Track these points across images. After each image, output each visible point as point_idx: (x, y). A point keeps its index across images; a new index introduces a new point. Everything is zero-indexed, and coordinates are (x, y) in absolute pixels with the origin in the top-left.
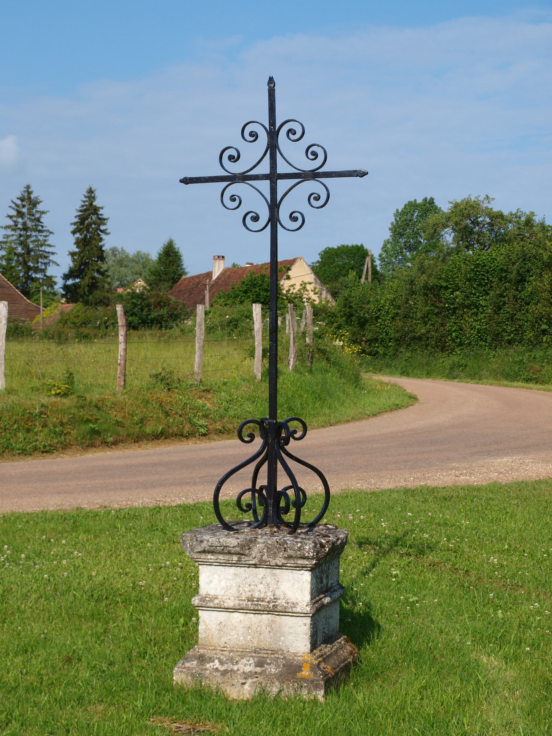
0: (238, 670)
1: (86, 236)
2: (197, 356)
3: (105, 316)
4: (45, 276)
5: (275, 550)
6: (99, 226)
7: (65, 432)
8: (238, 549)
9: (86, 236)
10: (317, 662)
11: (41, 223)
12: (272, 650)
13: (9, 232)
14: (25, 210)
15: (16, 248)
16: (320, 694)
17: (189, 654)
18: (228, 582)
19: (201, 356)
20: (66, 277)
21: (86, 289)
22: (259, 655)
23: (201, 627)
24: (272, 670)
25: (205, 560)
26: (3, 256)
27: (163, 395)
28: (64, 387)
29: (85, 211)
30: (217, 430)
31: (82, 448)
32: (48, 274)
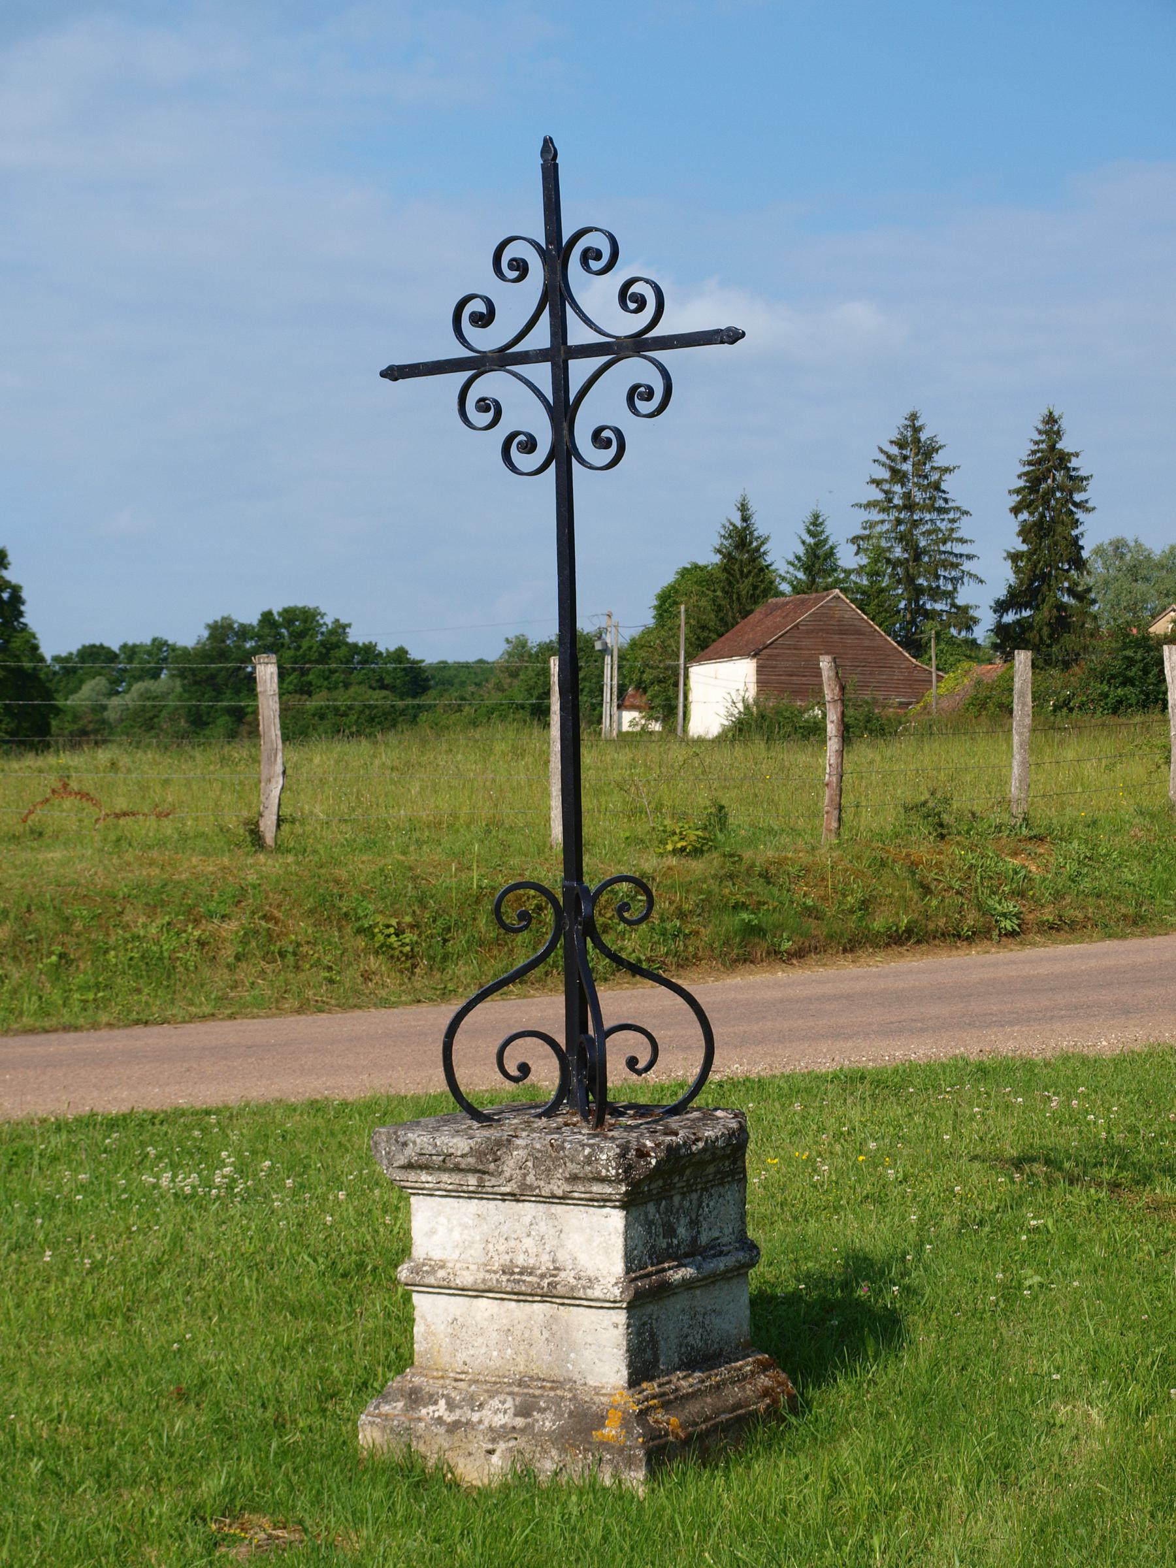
0: (480, 1422)
1: (1043, 516)
2: (1015, 764)
3: (1065, 687)
4: (953, 605)
5: (549, 1163)
6: (1071, 494)
7: (687, 931)
8: (472, 1160)
9: (1043, 516)
10: (637, 1409)
11: (944, 492)
12: (553, 1381)
13: (875, 515)
14: (907, 467)
15: (889, 549)
16: (636, 1478)
17: (391, 1387)
18: (466, 1232)
19: (1024, 763)
20: (1001, 607)
21: (1046, 631)
22: (526, 1391)
23: (418, 1330)
24: (547, 1422)
25: (417, 1185)
26: (862, 567)
27: (923, 849)
28: (692, 835)
29: (1039, 462)
30: (1043, 923)
31: (724, 965)
32: (960, 601)
